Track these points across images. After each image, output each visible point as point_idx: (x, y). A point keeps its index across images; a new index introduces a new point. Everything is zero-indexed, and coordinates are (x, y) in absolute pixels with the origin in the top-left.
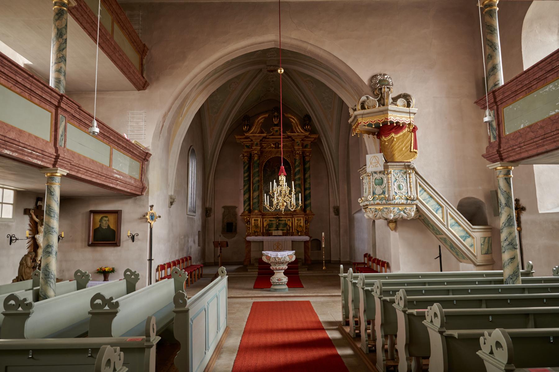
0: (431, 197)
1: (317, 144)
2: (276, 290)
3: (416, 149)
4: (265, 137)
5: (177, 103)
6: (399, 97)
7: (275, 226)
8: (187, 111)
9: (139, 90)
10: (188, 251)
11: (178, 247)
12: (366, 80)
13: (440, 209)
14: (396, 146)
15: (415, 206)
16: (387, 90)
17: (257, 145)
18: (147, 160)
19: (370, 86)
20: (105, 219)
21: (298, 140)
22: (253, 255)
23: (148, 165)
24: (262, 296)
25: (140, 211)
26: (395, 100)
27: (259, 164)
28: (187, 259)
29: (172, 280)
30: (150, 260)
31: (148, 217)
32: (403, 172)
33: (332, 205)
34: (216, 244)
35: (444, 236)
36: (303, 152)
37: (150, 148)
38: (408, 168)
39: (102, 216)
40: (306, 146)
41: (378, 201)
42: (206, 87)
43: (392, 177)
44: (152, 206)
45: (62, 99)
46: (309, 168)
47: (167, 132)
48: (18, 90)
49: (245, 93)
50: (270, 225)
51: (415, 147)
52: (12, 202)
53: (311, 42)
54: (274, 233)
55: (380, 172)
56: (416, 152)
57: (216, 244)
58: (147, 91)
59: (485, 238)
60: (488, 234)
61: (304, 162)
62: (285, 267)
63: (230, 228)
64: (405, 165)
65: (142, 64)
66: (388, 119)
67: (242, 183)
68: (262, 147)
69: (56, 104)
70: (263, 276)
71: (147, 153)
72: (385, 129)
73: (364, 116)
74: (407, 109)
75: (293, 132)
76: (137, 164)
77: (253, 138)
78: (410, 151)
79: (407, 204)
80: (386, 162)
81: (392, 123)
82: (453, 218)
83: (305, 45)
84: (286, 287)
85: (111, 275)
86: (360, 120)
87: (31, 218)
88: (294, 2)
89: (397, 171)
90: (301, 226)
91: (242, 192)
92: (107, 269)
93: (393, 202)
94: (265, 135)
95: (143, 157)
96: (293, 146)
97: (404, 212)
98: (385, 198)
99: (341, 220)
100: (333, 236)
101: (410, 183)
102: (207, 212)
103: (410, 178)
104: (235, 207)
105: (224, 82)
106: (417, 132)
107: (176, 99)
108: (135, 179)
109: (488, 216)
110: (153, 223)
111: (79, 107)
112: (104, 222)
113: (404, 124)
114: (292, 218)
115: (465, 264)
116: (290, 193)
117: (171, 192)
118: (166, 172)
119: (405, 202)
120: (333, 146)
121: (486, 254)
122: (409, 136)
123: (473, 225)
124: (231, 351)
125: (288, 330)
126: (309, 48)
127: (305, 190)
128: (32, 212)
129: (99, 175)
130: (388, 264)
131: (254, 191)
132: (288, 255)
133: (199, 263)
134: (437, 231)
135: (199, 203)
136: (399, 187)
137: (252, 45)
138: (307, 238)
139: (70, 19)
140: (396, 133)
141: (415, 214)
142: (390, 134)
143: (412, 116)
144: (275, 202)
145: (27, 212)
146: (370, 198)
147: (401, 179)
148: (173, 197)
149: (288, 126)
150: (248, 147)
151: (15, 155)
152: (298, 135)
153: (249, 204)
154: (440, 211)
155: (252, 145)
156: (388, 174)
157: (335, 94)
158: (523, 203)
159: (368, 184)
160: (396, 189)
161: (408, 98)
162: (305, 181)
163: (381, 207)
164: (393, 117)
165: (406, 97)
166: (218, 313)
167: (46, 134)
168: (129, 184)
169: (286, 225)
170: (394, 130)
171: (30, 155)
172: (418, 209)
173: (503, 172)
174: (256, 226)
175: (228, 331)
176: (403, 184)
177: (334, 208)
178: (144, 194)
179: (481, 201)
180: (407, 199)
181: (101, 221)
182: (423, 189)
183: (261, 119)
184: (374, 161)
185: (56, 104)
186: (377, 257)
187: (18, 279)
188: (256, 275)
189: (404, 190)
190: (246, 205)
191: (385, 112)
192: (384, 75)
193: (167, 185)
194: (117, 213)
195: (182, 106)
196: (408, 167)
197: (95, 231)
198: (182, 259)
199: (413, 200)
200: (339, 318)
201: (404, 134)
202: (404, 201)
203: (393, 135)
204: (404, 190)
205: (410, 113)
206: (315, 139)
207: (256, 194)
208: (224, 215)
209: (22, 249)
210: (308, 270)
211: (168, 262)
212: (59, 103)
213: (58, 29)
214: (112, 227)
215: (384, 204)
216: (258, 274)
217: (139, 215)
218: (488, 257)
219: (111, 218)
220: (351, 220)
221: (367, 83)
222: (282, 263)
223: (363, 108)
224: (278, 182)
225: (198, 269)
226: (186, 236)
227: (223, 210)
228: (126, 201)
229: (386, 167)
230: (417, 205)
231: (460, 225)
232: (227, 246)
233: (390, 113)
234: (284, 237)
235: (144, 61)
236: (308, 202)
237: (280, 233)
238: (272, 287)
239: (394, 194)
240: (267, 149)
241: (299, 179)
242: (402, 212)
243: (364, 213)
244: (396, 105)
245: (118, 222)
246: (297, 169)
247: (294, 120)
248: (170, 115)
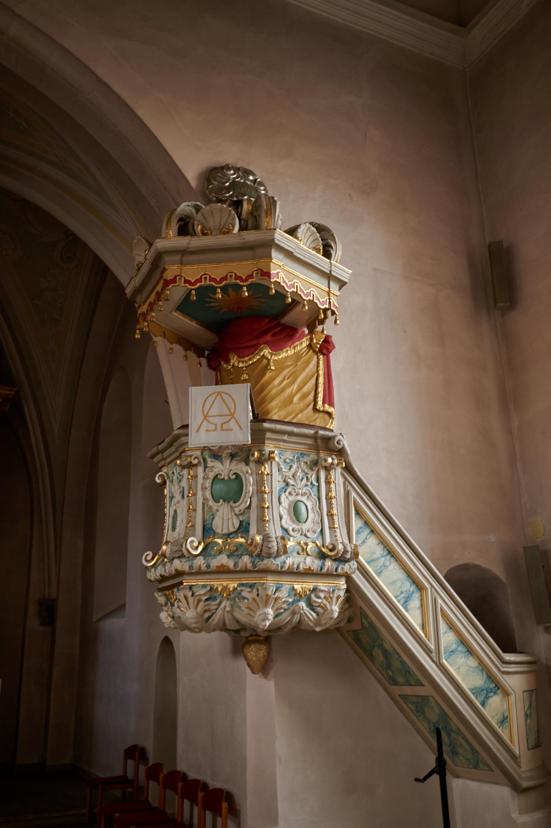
0: (391, 553)
3: (331, 404)
12: (192, 171)
13: (416, 596)
15: (342, 583)
32: (306, 459)
35: (426, 690)
38: (324, 448)
41: (223, 560)
51: (329, 399)
56: (330, 414)
64: (315, 437)
66: (268, 275)
73: (186, 258)
78: (315, 410)
82: (452, 626)
86: (172, 271)
89: (289, 455)
93: (279, 561)
97: (310, 605)
98: (249, 549)
101: (329, 499)
103: (328, 483)
115: (473, 785)
121: (534, 748)
123: (504, 652)
130: (229, 797)
136: (294, 511)
140: (277, 347)
146: (194, 545)
147: (301, 486)
154: (415, 603)
156: (260, 462)
157: (85, 246)
159: (186, 502)
160: (285, 517)
161: (327, 236)
170: (268, 338)
172: (352, 590)
179: (496, 578)
180: (322, 556)
182: (367, 523)
186: (181, 767)
191: (258, 251)
199: (341, 559)
201: (298, 356)
203: (266, 352)
215: (245, 571)
220: (88, 639)
221: (193, 183)
230: (349, 579)
231: (470, 651)
239: (280, 533)
243: (160, 608)
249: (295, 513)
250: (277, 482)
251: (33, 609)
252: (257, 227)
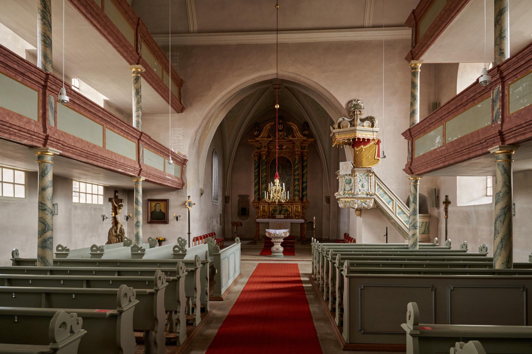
0: (385, 193)
1: (314, 146)
2: (274, 256)
4: (270, 141)
5: (205, 122)
7: (278, 211)
8: (212, 125)
9: (178, 113)
10: (212, 229)
12: (344, 104)
14: (364, 155)
16: (358, 113)
19: (347, 109)
22: (261, 233)
23: (186, 167)
24: (265, 260)
25: (182, 200)
26: (362, 120)
27: (266, 162)
28: (212, 235)
29: (207, 244)
30: (189, 233)
34: (233, 224)
35: (393, 221)
37: (187, 155)
39: (155, 203)
40: (304, 148)
41: (347, 196)
42: (226, 105)
43: (358, 178)
44: (189, 197)
45: (141, 135)
47: (198, 143)
48: (122, 134)
49: (256, 106)
50: (275, 211)
52: (23, 183)
53: (304, 75)
55: (349, 175)
57: (233, 224)
60: (426, 220)
61: (302, 160)
63: (244, 212)
65: (180, 94)
67: (253, 177)
68: (269, 148)
69: (138, 138)
70: (267, 247)
71: (185, 159)
72: (356, 143)
74: (371, 129)
75: (294, 137)
76: (179, 167)
79: (367, 198)
80: (354, 167)
81: (359, 139)
82: (400, 208)
83: (299, 77)
84: (282, 254)
85: (163, 243)
87: (113, 205)
88: (291, 43)
89: (361, 174)
90: (298, 212)
91: (253, 183)
92: (161, 239)
94: (271, 139)
95: (182, 162)
96: (294, 147)
97: (365, 204)
98: (353, 194)
99: (331, 208)
100: (324, 220)
102: (226, 200)
104: (248, 196)
106: (380, 144)
107: (204, 120)
109: (429, 207)
110: (190, 208)
111: (150, 138)
112: (157, 207)
113: (369, 140)
114: (292, 205)
116: (282, 189)
117: (201, 186)
119: (365, 196)
120: (327, 148)
122: (374, 148)
124: (242, 283)
125: (277, 276)
126: (302, 79)
127: (303, 183)
128: (113, 200)
129: (160, 178)
131: (262, 184)
132: (283, 233)
133: (220, 238)
134: (389, 218)
137: (259, 77)
138: (302, 221)
139: (142, 80)
140: (365, 145)
141: (373, 205)
142: (360, 145)
143: (375, 134)
144: (271, 195)
147: (364, 180)
148: (203, 190)
149: (289, 131)
150: (258, 148)
151: (123, 171)
152: (298, 140)
153: (259, 194)
154: (391, 203)
156: (355, 176)
158: (450, 199)
162: (303, 176)
163: (349, 200)
164: (360, 135)
165: (371, 119)
168: (175, 182)
169: (287, 210)
172: (375, 202)
173: (413, 181)
174: (264, 211)
176: (366, 184)
177: (326, 197)
178: (184, 188)
181: (155, 206)
182: (380, 187)
183: (268, 126)
185: (138, 138)
187: (108, 243)
189: (366, 188)
192: (358, 100)
193: (199, 181)
194: (166, 201)
195: (208, 122)
197: (152, 213)
198: (209, 234)
199: (371, 195)
200: (311, 272)
201: (371, 146)
202: (365, 196)
203: (362, 146)
204: (366, 188)
205: (373, 131)
206: (312, 142)
207: (264, 186)
208: (239, 202)
209: (108, 224)
210: (302, 244)
211: (200, 235)
212: (140, 137)
214: (163, 210)
217: (180, 203)
219: (162, 204)
222: (280, 238)
223: (339, 127)
224: (274, 183)
226: (212, 218)
228: (171, 193)
229: (353, 171)
230: (374, 199)
232: (242, 225)
233: (357, 132)
234: (285, 220)
236: (304, 193)
237: (282, 216)
240: (273, 150)
241: (298, 174)
242: (364, 204)
244: (363, 126)
245: (167, 207)
246: (297, 167)
247: (295, 127)
248: (200, 131)
249: (362, 186)
251: (324, 199)
252: (354, 126)
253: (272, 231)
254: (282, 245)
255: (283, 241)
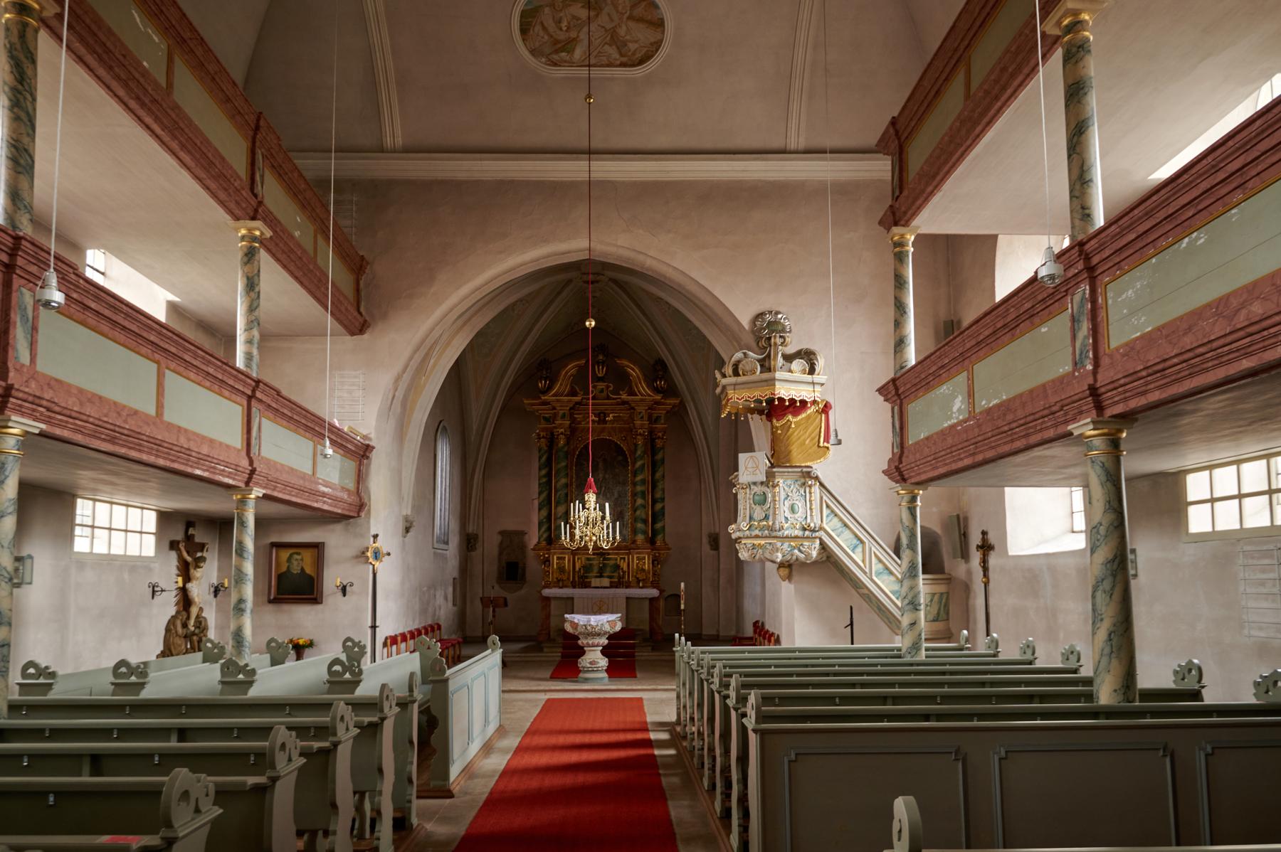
0: (846, 525)
1: (679, 415)
2: (586, 680)
6: (799, 354)
7: (596, 569)
9: (352, 334)
11: (417, 607)
12: (745, 322)
14: (794, 438)
16: (779, 341)
17: (563, 417)
18: (368, 458)
19: (753, 332)
20: (296, 557)
21: (641, 409)
23: (369, 465)
24: (564, 690)
26: (789, 358)
28: (432, 629)
30: (374, 627)
31: (369, 554)
33: (705, 532)
34: (486, 602)
35: (865, 591)
36: (651, 432)
37: (372, 436)
38: (807, 476)
40: (657, 420)
41: (757, 532)
44: (376, 536)
45: (257, 386)
46: (663, 460)
48: (208, 384)
50: (588, 568)
54: (595, 582)
55: (762, 483)
57: (486, 602)
58: (366, 336)
59: (934, 594)
60: (941, 588)
61: (652, 448)
62: (604, 641)
63: (512, 572)
65: (358, 290)
67: (535, 488)
68: (573, 420)
69: (249, 393)
70: (568, 658)
71: (368, 446)
72: (776, 409)
74: (809, 378)
75: (632, 393)
76: (351, 465)
77: (557, 405)
80: (772, 466)
82: (880, 561)
83: (641, 258)
84: (605, 675)
85: (307, 651)
86: (731, 393)
87: (180, 558)
89: (789, 482)
90: (643, 570)
91: (536, 503)
92: (301, 642)
95: (360, 453)
99: (722, 560)
100: (707, 590)
102: (469, 542)
104: (523, 533)
105: (501, 307)
107: (415, 352)
108: (348, 490)
110: (377, 564)
111: (279, 393)
112: (295, 563)
113: (804, 403)
114: (628, 554)
117: (407, 511)
118: (398, 473)
120: (710, 418)
126: (649, 262)
127: (654, 502)
128: (182, 546)
131: (557, 504)
132: (608, 622)
133: (454, 637)
134: (856, 584)
135: (454, 526)
137: (548, 256)
138: (654, 592)
139: (263, 255)
140: (795, 414)
141: (819, 554)
143: (818, 388)
145: (173, 545)
147: (795, 496)
149: (622, 380)
151: (206, 474)
153: (549, 529)
154: (859, 549)
155: (555, 416)
156: (774, 486)
162: (654, 486)
164: (784, 391)
165: (808, 356)
166: (489, 711)
167: (237, 441)
171: (222, 473)
172: (823, 546)
173: (907, 498)
174: (561, 569)
175: (501, 731)
176: (800, 505)
177: (710, 536)
178: (363, 514)
182: (833, 511)
183: (571, 368)
184: (751, 467)
185: (249, 393)
187: (163, 654)
188: (559, 659)
190: (543, 529)
192: (777, 313)
193: (400, 498)
194: (318, 547)
196: (808, 475)
199: (814, 531)
201: (809, 417)
202: (799, 533)
203: (790, 417)
204: (800, 514)
205: (813, 383)
206: (674, 406)
207: (561, 509)
209: (167, 606)
210: (654, 649)
211: (401, 630)
212: (254, 391)
213: (248, 278)
214: (308, 570)
216: (563, 657)
218: (940, 626)
219: (307, 556)
221: (747, 327)
222: (599, 635)
223: (736, 373)
224: (583, 503)
225: (453, 645)
226: (432, 587)
227: (500, 538)
229: (770, 475)
232: (506, 604)
233: (778, 385)
234: (613, 591)
235: (362, 283)
236: (658, 525)
237: (606, 582)
238: (581, 675)
241: (643, 482)
242: (796, 551)
244: (790, 371)
245: (319, 562)
246: (639, 464)
247: (634, 372)
250: (783, 495)
253: (579, 619)
254: (605, 652)
255: (606, 642)
